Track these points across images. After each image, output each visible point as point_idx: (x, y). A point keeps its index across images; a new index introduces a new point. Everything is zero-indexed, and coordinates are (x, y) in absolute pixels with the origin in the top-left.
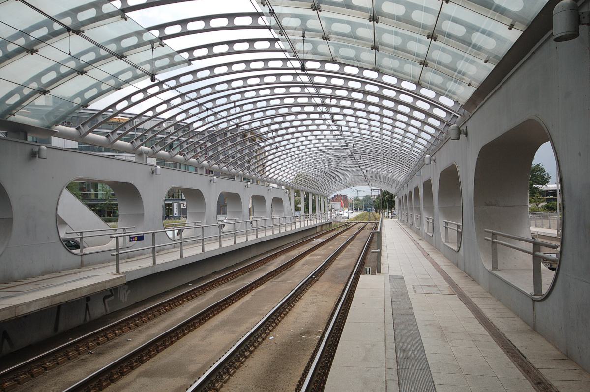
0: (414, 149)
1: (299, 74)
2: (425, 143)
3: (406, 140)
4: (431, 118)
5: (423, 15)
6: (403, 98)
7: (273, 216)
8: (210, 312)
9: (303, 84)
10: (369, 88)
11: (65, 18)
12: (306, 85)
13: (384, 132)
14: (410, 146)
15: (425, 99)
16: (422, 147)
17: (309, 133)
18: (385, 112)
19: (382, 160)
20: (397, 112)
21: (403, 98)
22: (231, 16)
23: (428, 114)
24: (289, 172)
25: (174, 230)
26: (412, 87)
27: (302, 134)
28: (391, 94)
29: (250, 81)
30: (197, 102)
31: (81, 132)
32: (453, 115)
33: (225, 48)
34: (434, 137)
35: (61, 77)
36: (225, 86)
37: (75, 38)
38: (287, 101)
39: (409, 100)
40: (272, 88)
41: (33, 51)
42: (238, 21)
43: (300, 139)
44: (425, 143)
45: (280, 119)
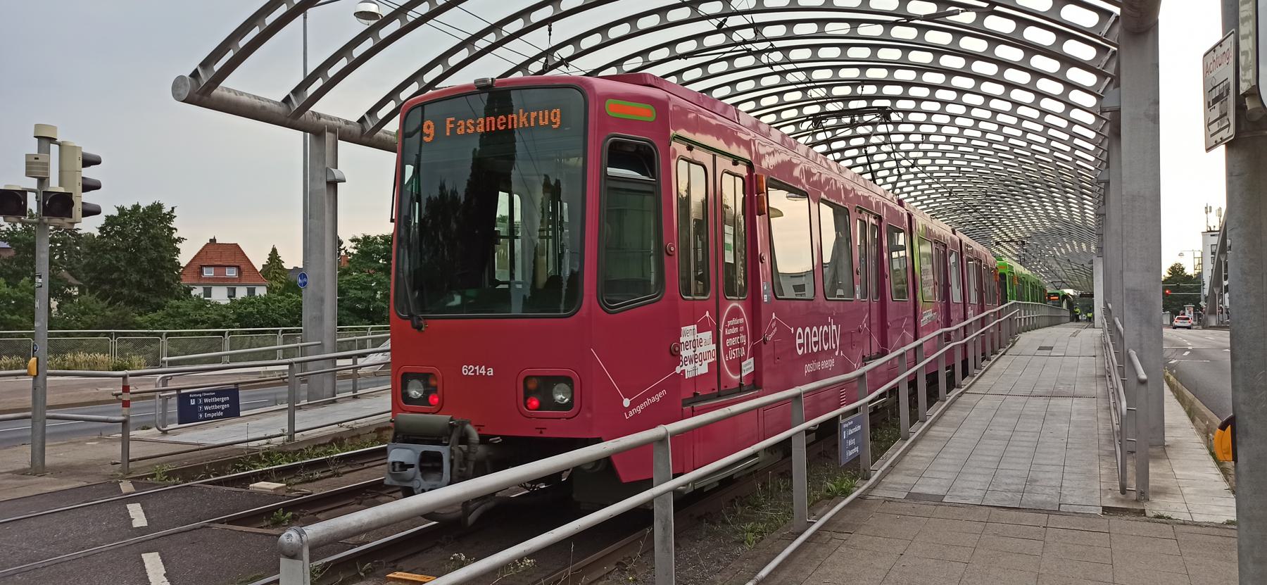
4: (550, 15)
5: (50, 444)
17: (998, 89)
22: (662, 11)
24: (975, 113)
25: (156, 408)
27: (978, 85)
29: (830, 28)
40: (844, 47)
42: (643, 24)
43: (968, 98)
45: (909, 75)
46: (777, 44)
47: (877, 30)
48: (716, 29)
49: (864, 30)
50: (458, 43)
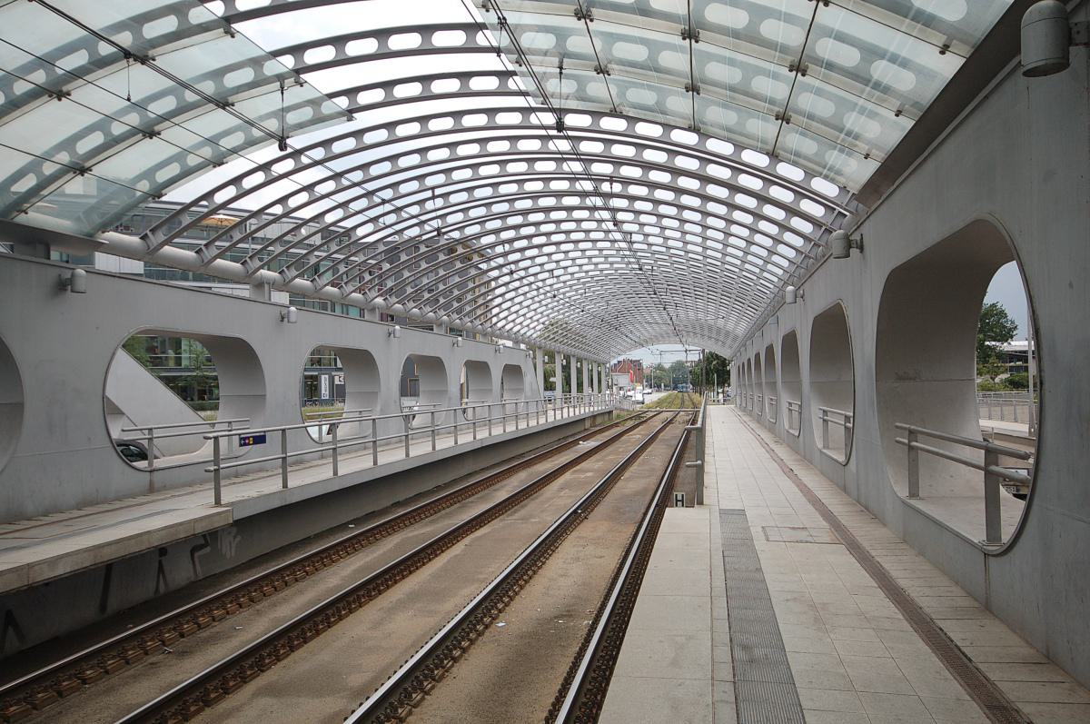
0: (765, 274)
1: (551, 137)
2: (785, 264)
3: (750, 258)
6: (745, 180)
7: (505, 398)
8: (387, 577)
9: (560, 156)
10: (681, 162)
11: (119, 33)
12: (565, 156)
13: (709, 243)
14: (757, 271)
15: (785, 183)
16: (780, 272)
17: (570, 246)
18: (712, 207)
19: (706, 295)
20: (733, 207)
21: (745, 180)
23: (791, 211)
25: (321, 425)
26: (761, 161)
27: (558, 248)
28: (723, 173)
29: (462, 151)
30: (363, 189)
31: (151, 245)
32: (836, 212)
33: (415, 89)
34: (802, 253)
35: (112, 143)
36: (415, 159)
37: (138, 70)
38: (529, 187)
39: (755, 184)
40: (503, 163)
41: (61, 95)
43: (555, 257)
44: (785, 264)
46: (438, 192)
47: (488, 191)
48: (354, 115)
49: (478, 193)
50: (174, 153)
